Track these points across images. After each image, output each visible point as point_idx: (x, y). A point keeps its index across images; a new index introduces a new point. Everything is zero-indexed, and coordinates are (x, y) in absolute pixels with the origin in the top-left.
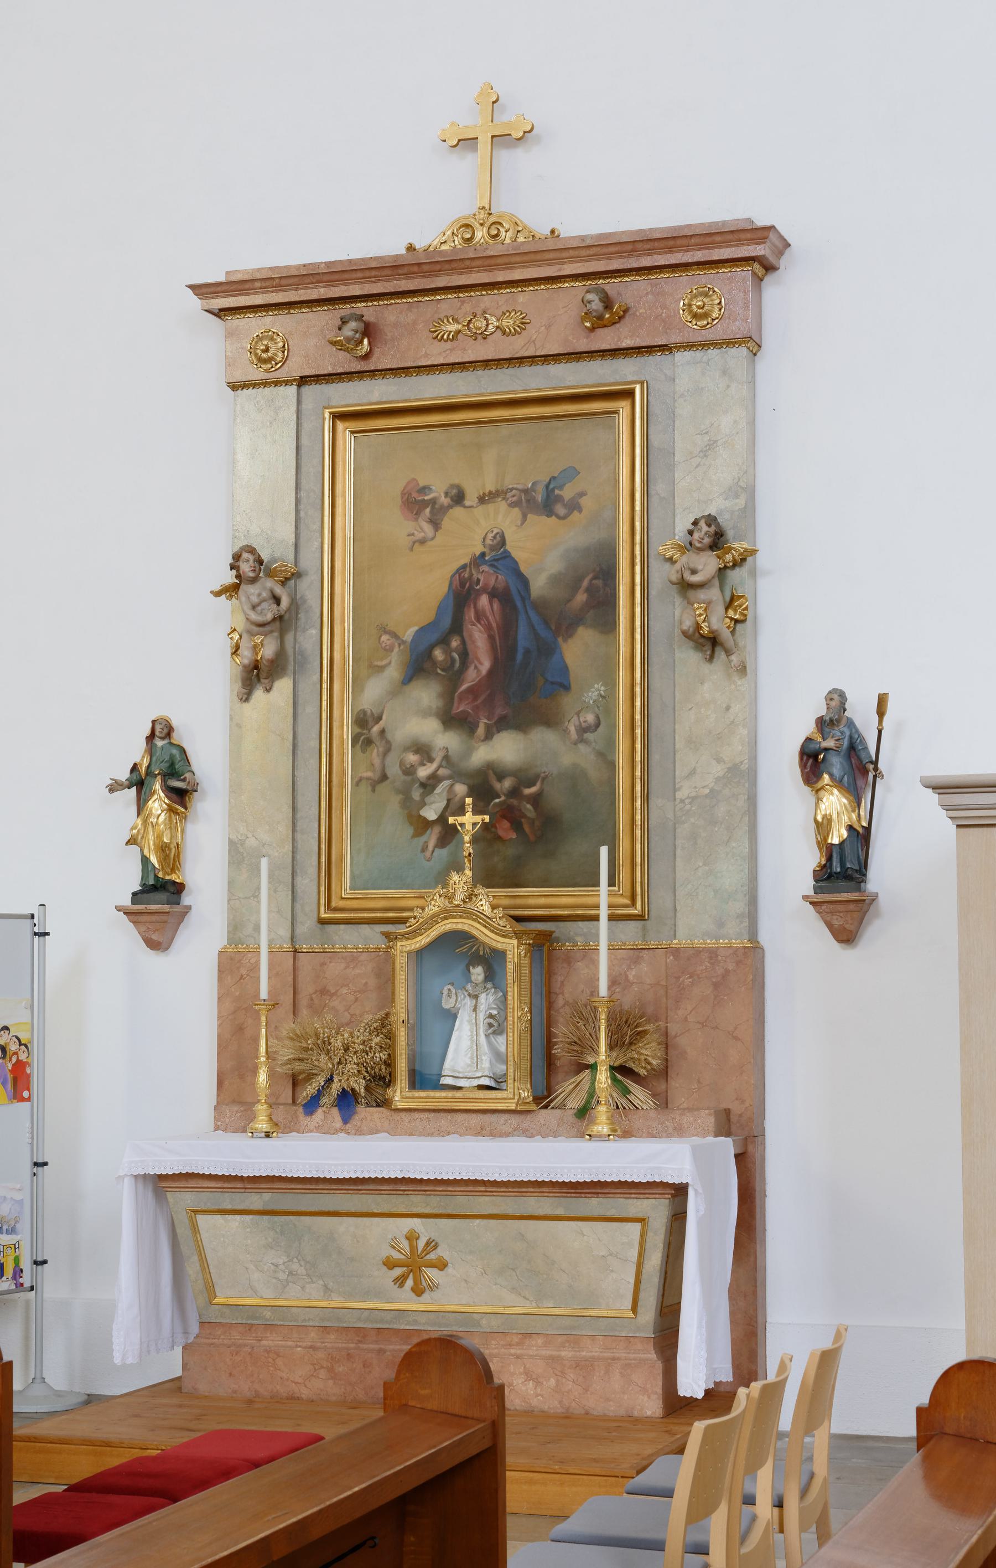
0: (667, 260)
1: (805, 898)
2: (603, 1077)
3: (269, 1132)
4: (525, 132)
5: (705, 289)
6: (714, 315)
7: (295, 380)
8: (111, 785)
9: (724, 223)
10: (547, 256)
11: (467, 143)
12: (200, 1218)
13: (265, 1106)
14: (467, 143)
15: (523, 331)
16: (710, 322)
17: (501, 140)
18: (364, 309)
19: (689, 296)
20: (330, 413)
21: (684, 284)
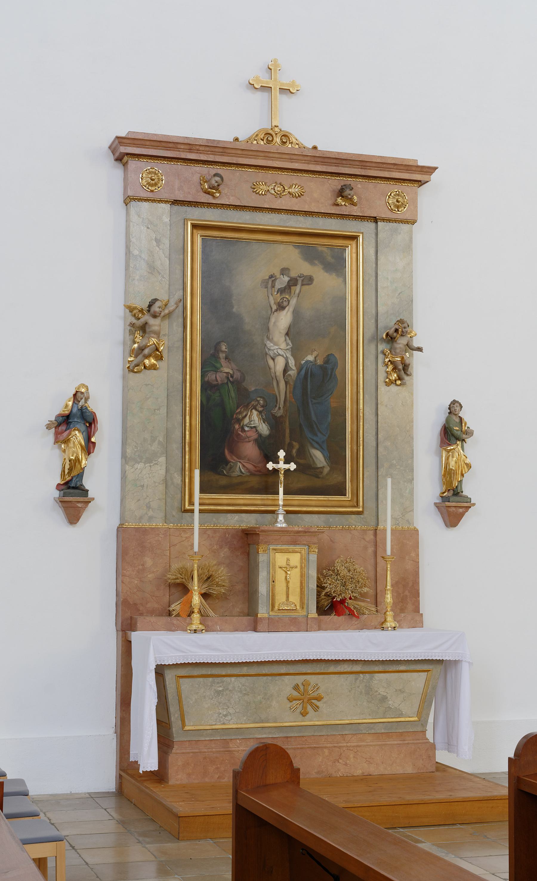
0: (200, 157)
1: (435, 504)
2: (196, 599)
3: (196, 630)
4: (253, 84)
5: (153, 170)
6: (159, 185)
7: (170, 201)
8: (48, 424)
9: (219, 141)
10: (271, 155)
11: (284, 91)
12: (182, 680)
13: (198, 615)
14: (284, 91)
15: (299, 198)
16: (157, 188)
17: (266, 89)
18: (352, 182)
19: (397, 193)
20: (191, 223)
21: (396, 188)
